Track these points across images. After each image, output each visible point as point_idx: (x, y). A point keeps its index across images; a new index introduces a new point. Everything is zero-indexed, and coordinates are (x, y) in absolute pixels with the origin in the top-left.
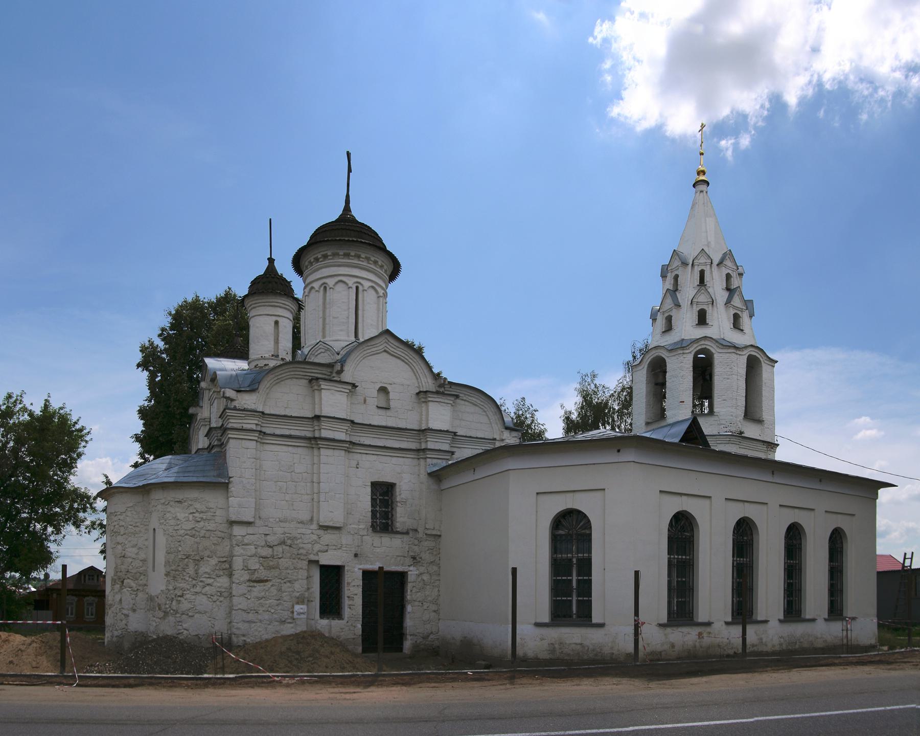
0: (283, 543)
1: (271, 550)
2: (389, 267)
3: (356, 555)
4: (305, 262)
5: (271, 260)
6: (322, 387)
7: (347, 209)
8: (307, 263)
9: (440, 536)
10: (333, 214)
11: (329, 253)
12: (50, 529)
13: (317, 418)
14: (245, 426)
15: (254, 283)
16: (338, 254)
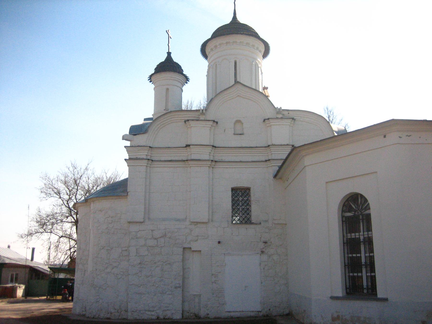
0: (164, 236)
1: (156, 241)
2: (262, 48)
3: (219, 242)
4: (208, 51)
5: (169, 54)
6: (192, 125)
7: (235, 17)
8: (210, 50)
9: (286, 224)
10: (228, 20)
11: (217, 44)
12: (357, 234)
13: (188, 146)
14: (139, 157)
15: (155, 69)
16: (229, 43)
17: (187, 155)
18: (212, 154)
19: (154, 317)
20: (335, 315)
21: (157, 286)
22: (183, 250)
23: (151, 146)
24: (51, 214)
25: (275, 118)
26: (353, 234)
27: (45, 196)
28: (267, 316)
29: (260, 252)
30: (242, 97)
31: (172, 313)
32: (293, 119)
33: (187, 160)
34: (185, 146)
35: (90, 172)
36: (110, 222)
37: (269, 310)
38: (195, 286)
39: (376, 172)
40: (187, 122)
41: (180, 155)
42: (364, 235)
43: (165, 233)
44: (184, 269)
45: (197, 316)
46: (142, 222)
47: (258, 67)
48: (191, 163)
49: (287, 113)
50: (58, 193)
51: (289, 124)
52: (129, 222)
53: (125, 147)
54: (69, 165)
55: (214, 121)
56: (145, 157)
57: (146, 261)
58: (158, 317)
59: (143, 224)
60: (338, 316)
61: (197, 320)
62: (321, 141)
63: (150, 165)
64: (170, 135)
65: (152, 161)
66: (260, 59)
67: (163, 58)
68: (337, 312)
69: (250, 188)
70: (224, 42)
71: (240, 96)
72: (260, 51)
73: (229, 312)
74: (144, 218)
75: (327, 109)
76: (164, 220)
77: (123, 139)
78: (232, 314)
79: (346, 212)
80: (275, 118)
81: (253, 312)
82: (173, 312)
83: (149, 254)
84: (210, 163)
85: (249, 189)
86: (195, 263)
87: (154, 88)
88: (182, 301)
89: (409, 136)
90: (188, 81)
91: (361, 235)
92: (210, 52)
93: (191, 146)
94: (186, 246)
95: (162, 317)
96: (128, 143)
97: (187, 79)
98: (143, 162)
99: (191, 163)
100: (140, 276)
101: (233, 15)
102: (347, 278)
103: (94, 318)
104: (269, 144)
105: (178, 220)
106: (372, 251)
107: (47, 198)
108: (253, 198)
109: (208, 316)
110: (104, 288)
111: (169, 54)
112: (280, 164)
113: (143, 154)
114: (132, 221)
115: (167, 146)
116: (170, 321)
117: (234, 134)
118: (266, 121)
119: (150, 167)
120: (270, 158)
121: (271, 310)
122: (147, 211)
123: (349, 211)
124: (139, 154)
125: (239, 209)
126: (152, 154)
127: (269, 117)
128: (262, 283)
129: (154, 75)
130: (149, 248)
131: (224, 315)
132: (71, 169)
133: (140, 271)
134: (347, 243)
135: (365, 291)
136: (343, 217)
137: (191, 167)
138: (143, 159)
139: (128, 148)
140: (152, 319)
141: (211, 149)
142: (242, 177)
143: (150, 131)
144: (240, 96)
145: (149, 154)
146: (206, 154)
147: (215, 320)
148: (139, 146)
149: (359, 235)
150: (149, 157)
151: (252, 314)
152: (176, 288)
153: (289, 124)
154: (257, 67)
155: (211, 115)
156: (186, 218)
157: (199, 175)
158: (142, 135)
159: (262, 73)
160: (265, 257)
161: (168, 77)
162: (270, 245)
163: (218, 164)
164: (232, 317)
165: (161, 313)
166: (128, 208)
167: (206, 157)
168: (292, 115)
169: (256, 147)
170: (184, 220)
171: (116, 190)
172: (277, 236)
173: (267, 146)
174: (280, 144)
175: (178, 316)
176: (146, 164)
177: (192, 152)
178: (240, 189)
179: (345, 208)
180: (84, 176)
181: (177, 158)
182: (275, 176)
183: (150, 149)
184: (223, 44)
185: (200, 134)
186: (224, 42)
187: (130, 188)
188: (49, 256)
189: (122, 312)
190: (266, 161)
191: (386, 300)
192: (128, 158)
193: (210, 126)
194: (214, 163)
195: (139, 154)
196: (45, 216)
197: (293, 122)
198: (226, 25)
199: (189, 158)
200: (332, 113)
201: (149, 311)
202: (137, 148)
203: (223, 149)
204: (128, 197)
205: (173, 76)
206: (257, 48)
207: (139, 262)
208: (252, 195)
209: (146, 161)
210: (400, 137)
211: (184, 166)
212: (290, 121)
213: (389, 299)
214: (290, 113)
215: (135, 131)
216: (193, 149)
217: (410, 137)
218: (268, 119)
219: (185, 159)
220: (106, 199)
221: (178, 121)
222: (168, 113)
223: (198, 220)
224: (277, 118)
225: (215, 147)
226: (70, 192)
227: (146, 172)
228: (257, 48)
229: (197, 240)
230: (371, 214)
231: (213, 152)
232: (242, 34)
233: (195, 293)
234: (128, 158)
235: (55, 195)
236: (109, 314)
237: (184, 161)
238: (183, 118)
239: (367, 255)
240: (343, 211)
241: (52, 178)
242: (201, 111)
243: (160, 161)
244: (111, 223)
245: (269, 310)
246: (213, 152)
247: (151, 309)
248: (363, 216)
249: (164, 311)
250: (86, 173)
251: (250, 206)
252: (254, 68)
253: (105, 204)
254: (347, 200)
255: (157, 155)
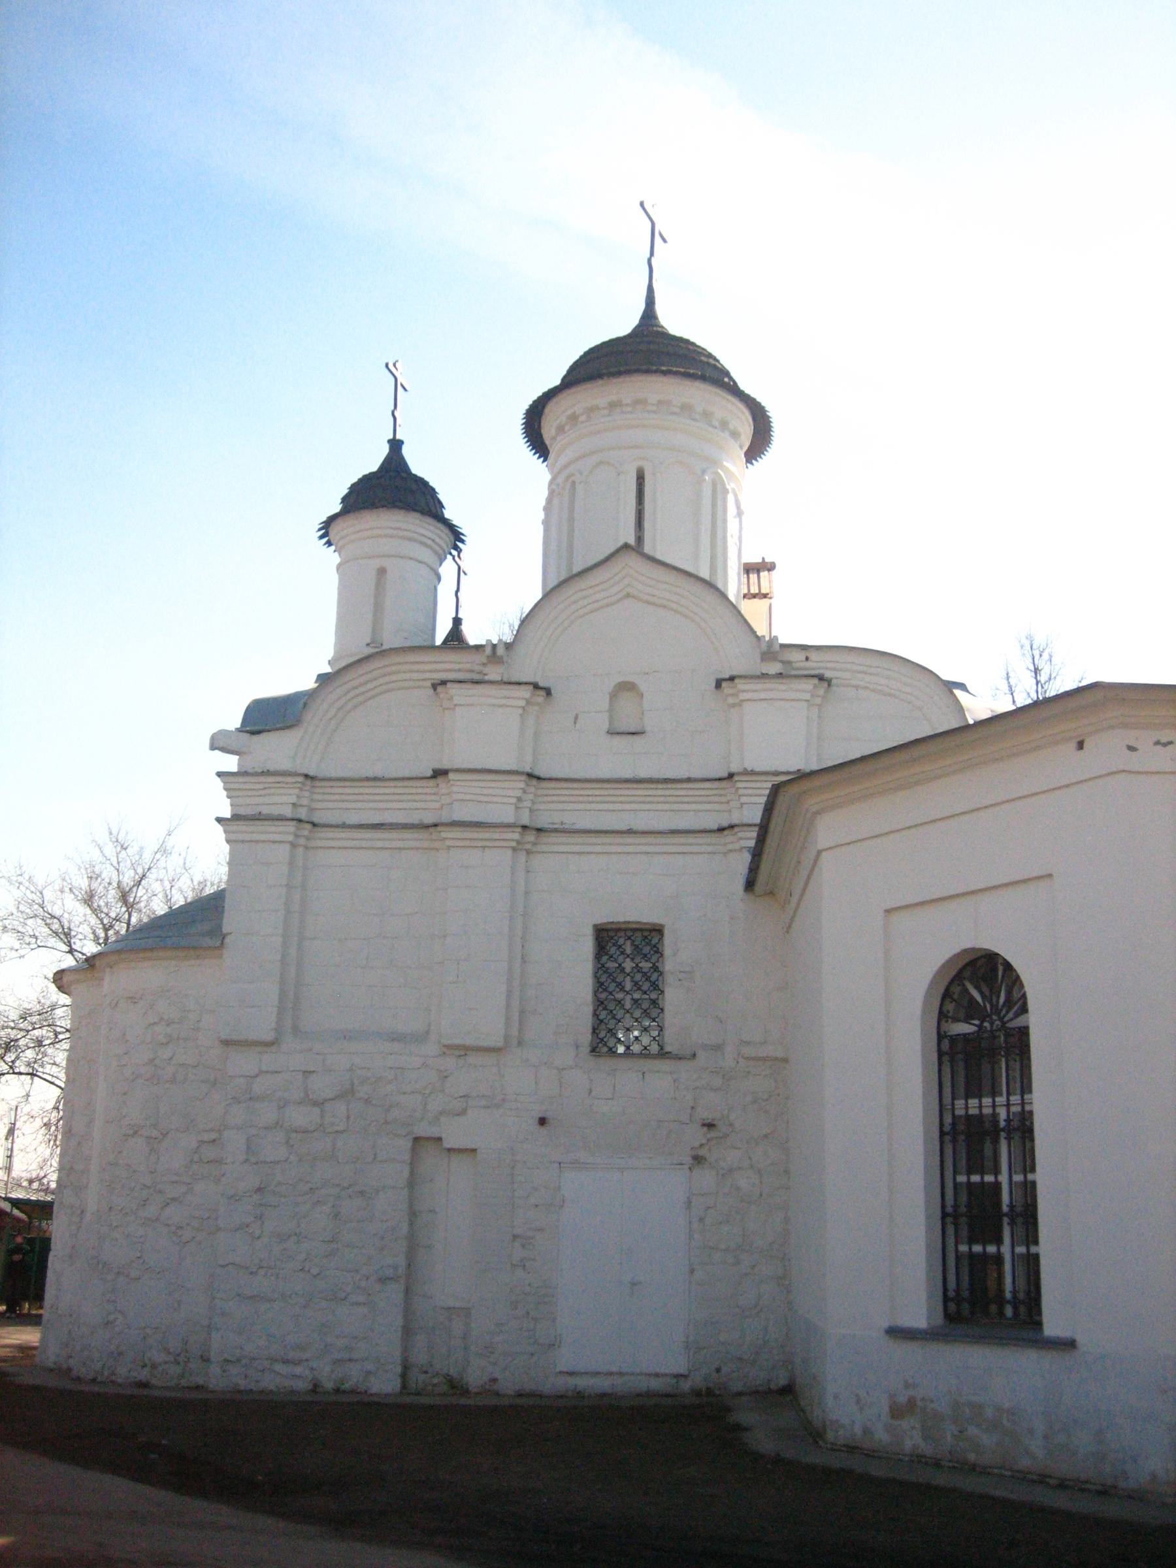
0: (347, 1093)
1: (317, 1110)
2: (745, 427)
3: (542, 1121)
4: (548, 430)
5: (396, 445)
6: (456, 700)
7: (649, 314)
9: (785, 1060)
10: (624, 324)
13: (439, 774)
14: (266, 810)
15: (344, 500)
17: (437, 805)
18: (529, 804)
19: (302, 1385)
20: (902, 1399)
21: (315, 1271)
22: (413, 1149)
23: (311, 774)
24: (38, 1007)
25: (758, 677)
26: (973, 1102)
27: (17, 945)
28: (709, 1392)
29: (688, 1160)
30: (640, 600)
31: (369, 1373)
32: (821, 678)
33: (436, 825)
34: (430, 773)
35: (173, 863)
36: (164, 1041)
37: (718, 1370)
38: (451, 1279)
39: (1050, 876)
40: (440, 689)
41: (416, 805)
42: (1008, 1105)
43: (352, 1084)
44: (413, 1214)
45: (455, 1386)
46: (272, 1044)
47: (726, 491)
48: (450, 835)
49: (801, 656)
50: (66, 935)
51: (807, 696)
52: (227, 1043)
53: (219, 774)
54: (103, 838)
55: (536, 686)
56: (288, 811)
57: (279, 1184)
58: (315, 1386)
59: (274, 1049)
60: (912, 1402)
61: (453, 1400)
62: (863, 759)
63: (308, 839)
64: (387, 735)
65: (314, 825)
66: (733, 463)
67: (372, 460)
68: (907, 1386)
69: (662, 926)
70: (602, 402)
71: (634, 597)
72: (735, 435)
73: (571, 1374)
74: (279, 1030)
75: (1030, 639)
76: (347, 1036)
77: (213, 747)
78: (582, 1383)
79: (956, 1020)
80: (758, 677)
81: (657, 1375)
82: (370, 1366)
83: (292, 1158)
84: (516, 836)
85: (658, 930)
86: (454, 1194)
87: (339, 567)
88: (404, 1327)
89: (1165, 745)
90: (463, 541)
91: (999, 1106)
92: (554, 438)
93: (451, 776)
94: (424, 1129)
95: (329, 1385)
96: (231, 763)
97: (456, 536)
98: (281, 829)
99: (450, 835)
100: (257, 1233)
101: (642, 306)
102: (951, 1262)
103: (94, 1380)
104: (734, 768)
105: (396, 1038)
106: (1029, 1165)
107: (22, 952)
108: (669, 965)
109: (495, 1387)
110: (133, 1274)
111: (396, 445)
112: (752, 843)
113: (282, 800)
114: (234, 1037)
115: (370, 774)
116: (354, 1399)
117: (612, 733)
118: (724, 684)
119: (306, 848)
120: (735, 821)
121: (725, 1370)
122: (290, 1002)
123: (967, 1019)
124: (267, 800)
125: (635, 1001)
126: (312, 800)
127: (735, 673)
128: (692, 1271)
129: (339, 521)
130: (294, 1135)
131: (552, 1384)
132: (110, 850)
133: (260, 1217)
134: (954, 1132)
135: (1009, 1311)
136: (941, 1036)
137: (449, 847)
138: (281, 819)
139: (232, 779)
140: (293, 1392)
141: (522, 785)
142: (631, 887)
143: (314, 719)
144: (634, 597)
145: (305, 802)
146: (500, 803)
147: (518, 1401)
148: (267, 773)
149: (994, 1106)
150: (302, 813)
151: (656, 1385)
152: (383, 1280)
153: (807, 696)
154: (718, 491)
155: (525, 667)
156: (428, 1032)
157: (478, 878)
158: (278, 734)
159: (740, 514)
160: (706, 1178)
161: (388, 526)
162: (726, 1136)
163: (544, 838)
164: (579, 1395)
165: (328, 1369)
166: (229, 989)
167: (507, 815)
168: (816, 664)
169: (689, 780)
170: (421, 1038)
171: (196, 926)
172: (754, 1102)
173: (725, 775)
174: (773, 769)
175: (385, 1384)
176: (291, 838)
177: (455, 796)
178: (625, 930)
179: (950, 1007)
180: (152, 876)
181: (400, 818)
182: (750, 885)
183: (309, 782)
184: (597, 408)
185: (486, 730)
186: (602, 402)
187: (230, 922)
188: (10, 1157)
189: (191, 1365)
190: (721, 830)
191: (1069, 1345)
192: (227, 814)
193: (523, 703)
194: (531, 837)
195: (267, 800)
196: (14, 1015)
197: (821, 691)
198: (604, 343)
199: (444, 819)
200: (1046, 656)
201: (286, 1362)
202: (262, 779)
203: (565, 785)
204: (226, 953)
205: (403, 525)
206: (724, 425)
207: (257, 1185)
208: (668, 951)
209: (291, 827)
210: (1131, 749)
211: (426, 844)
212: (809, 685)
213: (1080, 1339)
214: (813, 656)
215: (266, 717)
216: (458, 786)
217: (1170, 747)
218: (732, 679)
219: (429, 819)
220: (150, 959)
221: (412, 684)
222: (378, 653)
223: (469, 1041)
224: (764, 676)
225: (539, 778)
226: (106, 930)
227: (291, 864)
228: (724, 425)
229: (463, 1112)
230: (1031, 1031)
231: (531, 796)
232: (665, 373)
233: (451, 1303)
234: (227, 814)
235: (53, 942)
236: (146, 1371)
237: (427, 827)
238: (428, 675)
239: (1018, 1178)
240: (942, 1016)
241: (40, 881)
242: (488, 651)
243: (344, 826)
244: (168, 1043)
245: (718, 1370)
246: (531, 796)
247: (291, 1355)
248: (1007, 1035)
249: (338, 1362)
250: (162, 864)
251: (662, 992)
252: (707, 491)
253: (149, 975)
254: (958, 978)
255: (330, 805)
